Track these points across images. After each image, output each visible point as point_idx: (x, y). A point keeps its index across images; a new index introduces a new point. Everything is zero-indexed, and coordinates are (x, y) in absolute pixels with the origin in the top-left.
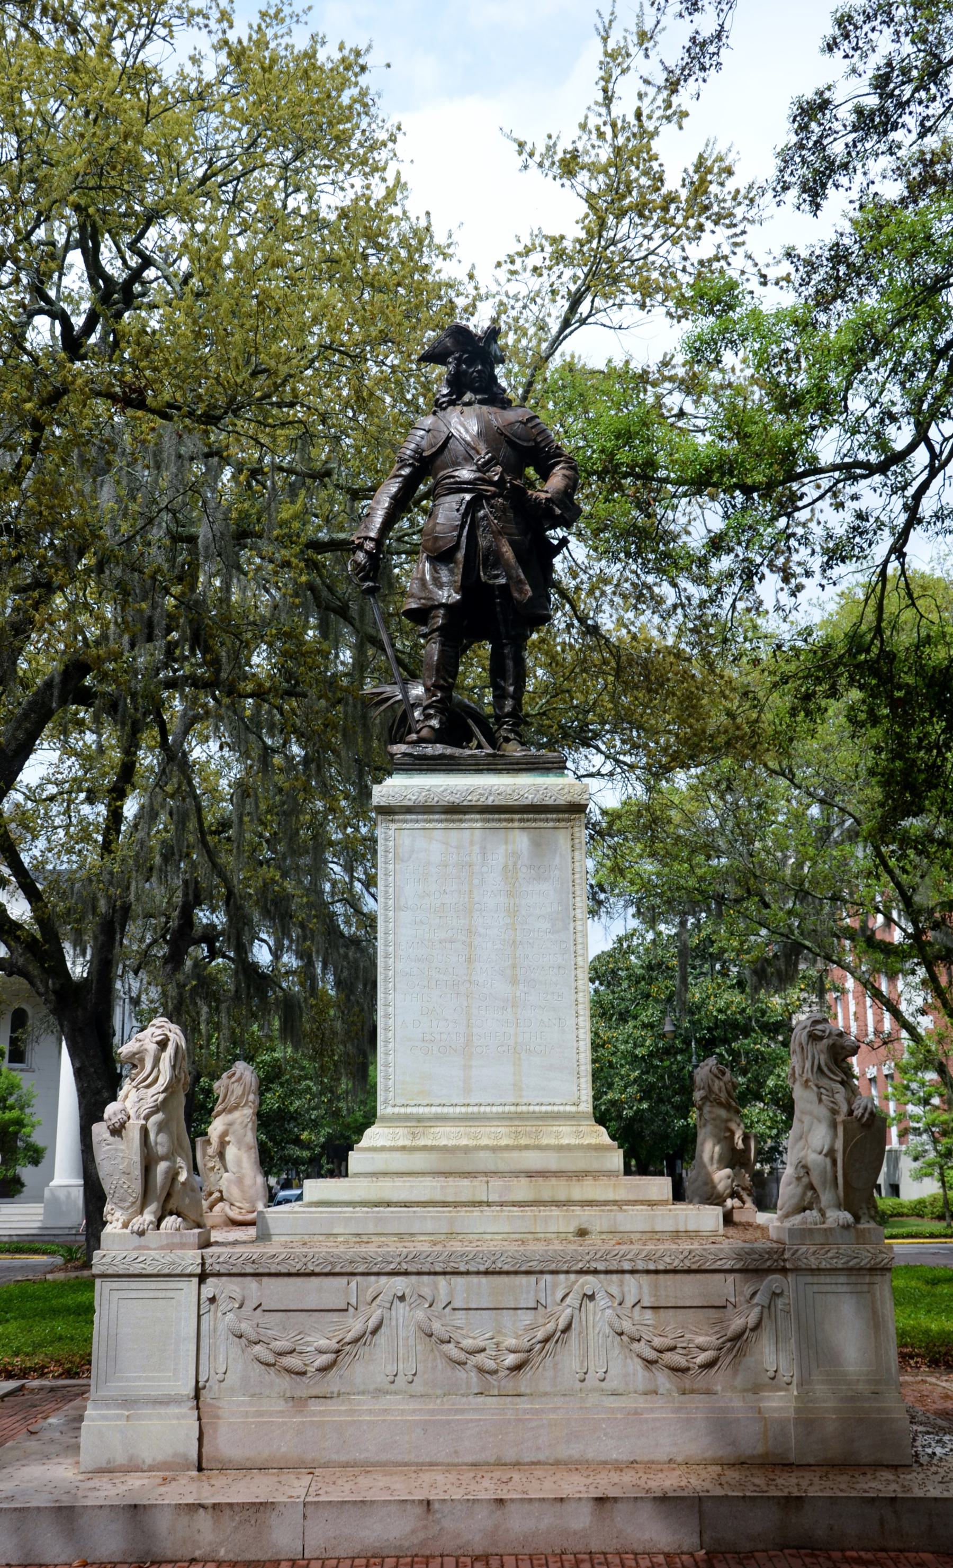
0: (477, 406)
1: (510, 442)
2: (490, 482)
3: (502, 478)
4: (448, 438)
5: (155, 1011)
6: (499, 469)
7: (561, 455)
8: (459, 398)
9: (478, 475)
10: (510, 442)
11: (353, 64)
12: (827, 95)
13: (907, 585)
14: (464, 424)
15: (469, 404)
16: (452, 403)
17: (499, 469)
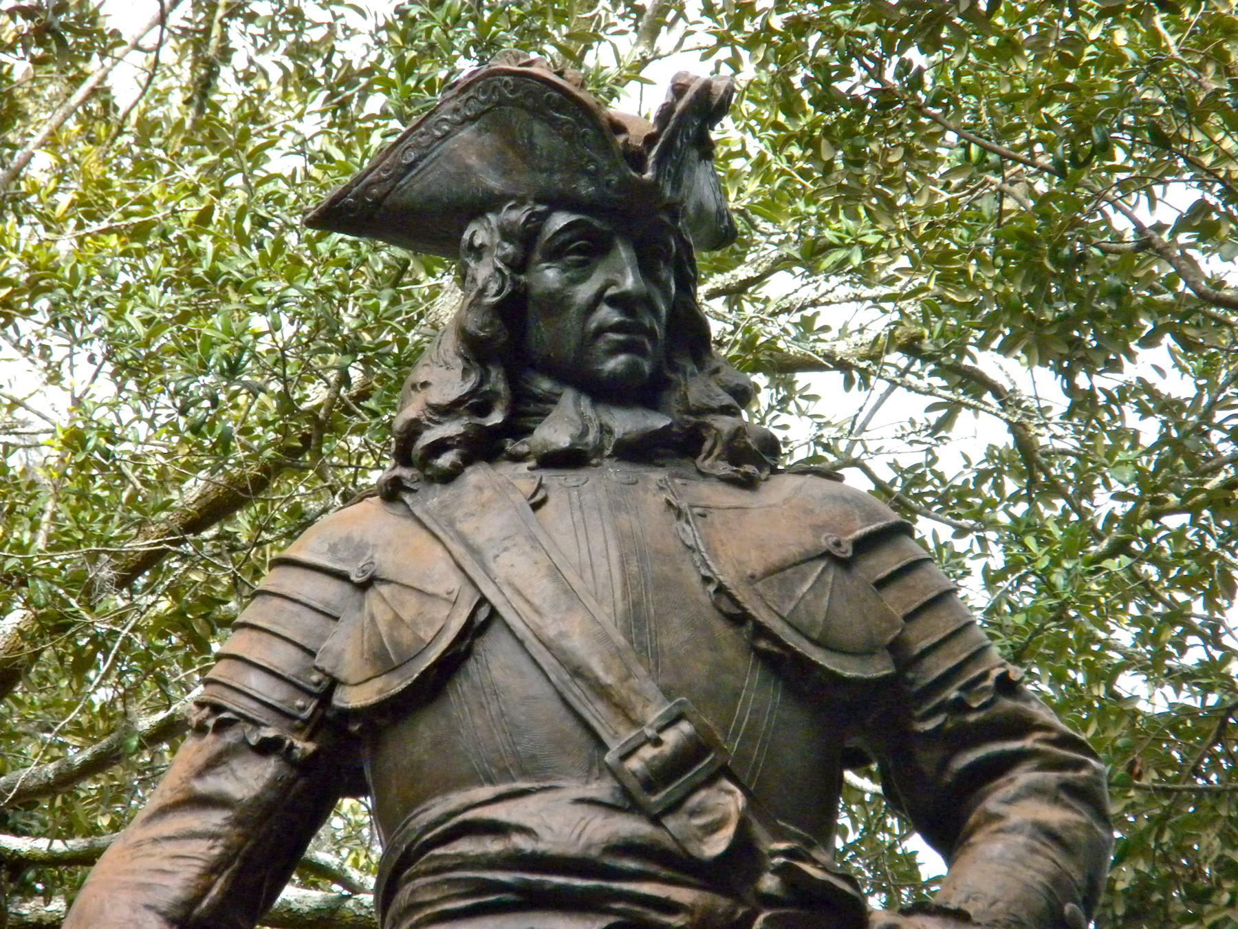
0: (614, 472)
1: (784, 666)
2: (680, 865)
3: (743, 846)
4: (481, 624)
5: (144, 300)
6: (729, 801)
7: (1022, 725)
8: (517, 427)
9: (630, 827)
10: (784, 666)
11: (234, 50)
12: (241, 75)
13: (411, 166)
14: (548, 556)
15: (569, 459)
16: (484, 448)
17: (729, 801)
